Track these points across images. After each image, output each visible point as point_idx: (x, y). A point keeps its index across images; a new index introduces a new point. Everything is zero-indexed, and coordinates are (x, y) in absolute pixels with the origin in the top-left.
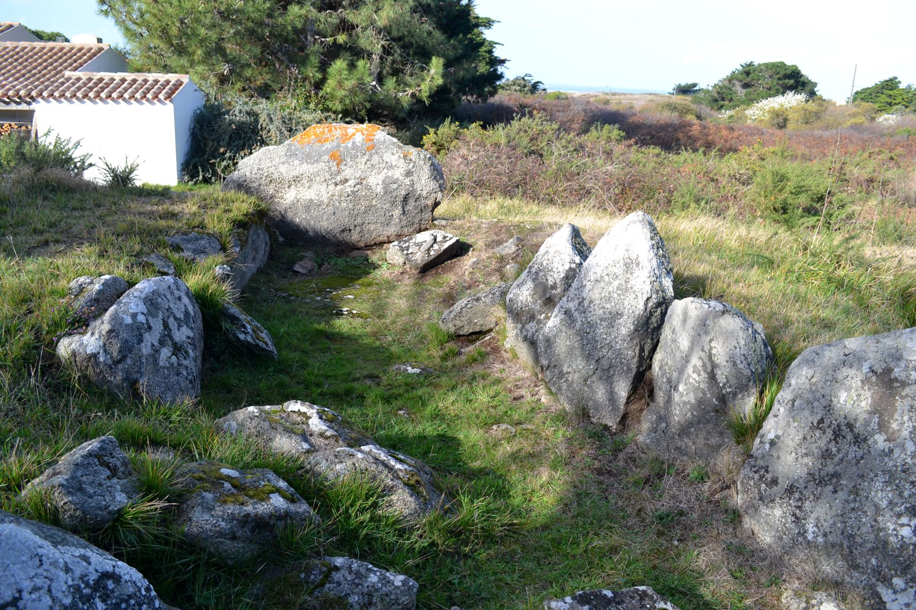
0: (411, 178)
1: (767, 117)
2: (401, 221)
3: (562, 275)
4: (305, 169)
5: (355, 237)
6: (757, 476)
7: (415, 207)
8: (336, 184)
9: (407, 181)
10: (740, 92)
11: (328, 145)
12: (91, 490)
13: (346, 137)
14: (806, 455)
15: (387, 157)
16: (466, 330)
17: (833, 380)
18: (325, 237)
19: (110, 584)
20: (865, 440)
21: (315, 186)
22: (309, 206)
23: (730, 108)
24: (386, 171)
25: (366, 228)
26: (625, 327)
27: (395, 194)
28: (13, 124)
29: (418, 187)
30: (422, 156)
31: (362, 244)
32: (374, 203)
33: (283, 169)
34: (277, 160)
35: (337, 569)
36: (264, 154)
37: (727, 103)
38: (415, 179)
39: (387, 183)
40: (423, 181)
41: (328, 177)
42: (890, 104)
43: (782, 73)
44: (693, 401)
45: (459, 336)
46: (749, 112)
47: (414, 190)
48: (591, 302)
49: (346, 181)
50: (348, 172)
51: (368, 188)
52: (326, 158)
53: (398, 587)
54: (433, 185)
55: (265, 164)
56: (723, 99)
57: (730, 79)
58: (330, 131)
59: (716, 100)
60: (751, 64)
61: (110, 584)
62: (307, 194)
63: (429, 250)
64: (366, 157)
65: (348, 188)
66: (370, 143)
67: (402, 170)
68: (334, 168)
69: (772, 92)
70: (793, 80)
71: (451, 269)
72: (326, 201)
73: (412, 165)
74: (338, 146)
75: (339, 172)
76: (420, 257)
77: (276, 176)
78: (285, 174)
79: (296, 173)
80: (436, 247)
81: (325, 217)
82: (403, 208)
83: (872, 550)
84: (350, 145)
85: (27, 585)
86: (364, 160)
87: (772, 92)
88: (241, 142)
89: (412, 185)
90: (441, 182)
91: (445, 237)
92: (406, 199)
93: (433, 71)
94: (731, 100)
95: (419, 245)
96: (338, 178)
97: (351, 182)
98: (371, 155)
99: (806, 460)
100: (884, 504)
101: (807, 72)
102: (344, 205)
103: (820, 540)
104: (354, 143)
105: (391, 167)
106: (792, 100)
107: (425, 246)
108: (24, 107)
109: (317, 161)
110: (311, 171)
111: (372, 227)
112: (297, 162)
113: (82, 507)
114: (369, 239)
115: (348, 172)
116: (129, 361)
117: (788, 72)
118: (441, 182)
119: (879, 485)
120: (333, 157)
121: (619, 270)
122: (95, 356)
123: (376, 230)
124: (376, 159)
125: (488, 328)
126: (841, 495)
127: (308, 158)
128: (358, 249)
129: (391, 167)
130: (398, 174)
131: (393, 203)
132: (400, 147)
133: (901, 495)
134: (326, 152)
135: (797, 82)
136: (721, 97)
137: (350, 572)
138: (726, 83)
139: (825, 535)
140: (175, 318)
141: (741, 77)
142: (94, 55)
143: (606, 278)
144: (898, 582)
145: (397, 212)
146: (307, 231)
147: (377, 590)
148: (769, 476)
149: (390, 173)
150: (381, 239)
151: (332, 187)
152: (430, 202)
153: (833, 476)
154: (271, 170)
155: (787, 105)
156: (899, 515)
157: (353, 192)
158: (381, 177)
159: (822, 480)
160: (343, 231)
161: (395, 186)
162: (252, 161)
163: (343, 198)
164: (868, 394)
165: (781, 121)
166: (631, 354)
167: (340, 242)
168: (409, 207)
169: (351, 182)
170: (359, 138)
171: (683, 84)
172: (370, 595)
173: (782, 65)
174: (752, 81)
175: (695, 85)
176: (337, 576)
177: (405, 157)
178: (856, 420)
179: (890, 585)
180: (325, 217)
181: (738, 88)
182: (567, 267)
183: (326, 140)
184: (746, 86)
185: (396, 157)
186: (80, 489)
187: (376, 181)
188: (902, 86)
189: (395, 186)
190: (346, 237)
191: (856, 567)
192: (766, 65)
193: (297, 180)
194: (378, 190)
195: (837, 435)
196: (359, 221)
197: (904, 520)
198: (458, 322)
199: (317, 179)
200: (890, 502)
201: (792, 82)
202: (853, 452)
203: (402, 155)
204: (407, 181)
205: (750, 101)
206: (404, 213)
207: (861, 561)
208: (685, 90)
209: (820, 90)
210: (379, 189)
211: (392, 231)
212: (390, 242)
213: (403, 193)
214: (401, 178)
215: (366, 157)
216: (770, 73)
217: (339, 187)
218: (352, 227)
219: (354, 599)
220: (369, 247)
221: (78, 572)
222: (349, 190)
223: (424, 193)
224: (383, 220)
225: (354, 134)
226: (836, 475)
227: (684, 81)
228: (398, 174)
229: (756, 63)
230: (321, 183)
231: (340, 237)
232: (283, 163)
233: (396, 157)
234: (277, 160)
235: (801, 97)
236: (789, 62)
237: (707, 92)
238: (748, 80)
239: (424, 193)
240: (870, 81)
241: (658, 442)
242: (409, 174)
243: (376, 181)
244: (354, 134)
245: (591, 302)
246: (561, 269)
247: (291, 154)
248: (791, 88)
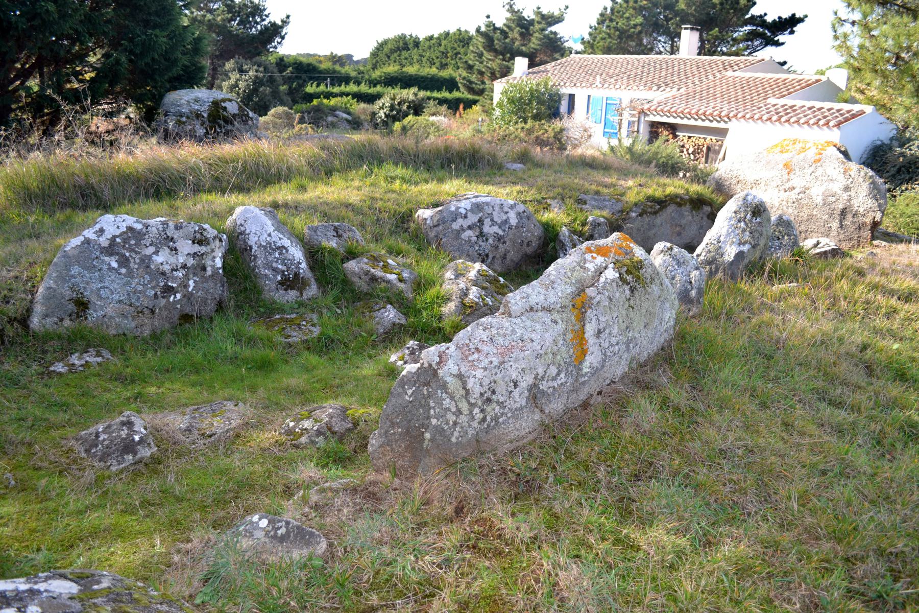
0: (849, 193)
7: (853, 223)
9: (845, 196)
12: (319, 234)
19: (284, 251)
28: (713, 138)
29: (855, 203)
30: (862, 173)
32: (815, 213)
38: (853, 193)
40: (860, 199)
47: (850, 206)
61: (284, 251)
64: (812, 169)
65: (793, 195)
68: (786, 176)
73: (851, 180)
77: (741, 178)
82: (841, 222)
85: (254, 231)
86: (810, 172)
88: (908, 177)
90: (882, 201)
92: (843, 213)
96: (787, 186)
102: (790, 211)
108: (722, 125)
113: (310, 236)
116: (441, 227)
118: (882, 201)
122: (426, 219)
124: (820, 171)
130: (837, 187)
132: (843, 163)
140: (492, 220)
142: (809, 85)
145: (835, 225)
157: (798, 200)
158: (823, 189)
161: (833, 199)
169: (797, 190)
186: (315, 231)
194: (818, 201)
203: (842, 171)
204: (845, 196)
206: (841, 227)
210: (819, 200)
213: (841, 206)
214: (839, 192)
215: (812, 169)
221: (274, 239)
224: (823, 230)
228: (837, 187)
239: (861, 210)
242: (847, 189)
243: (817, 193)
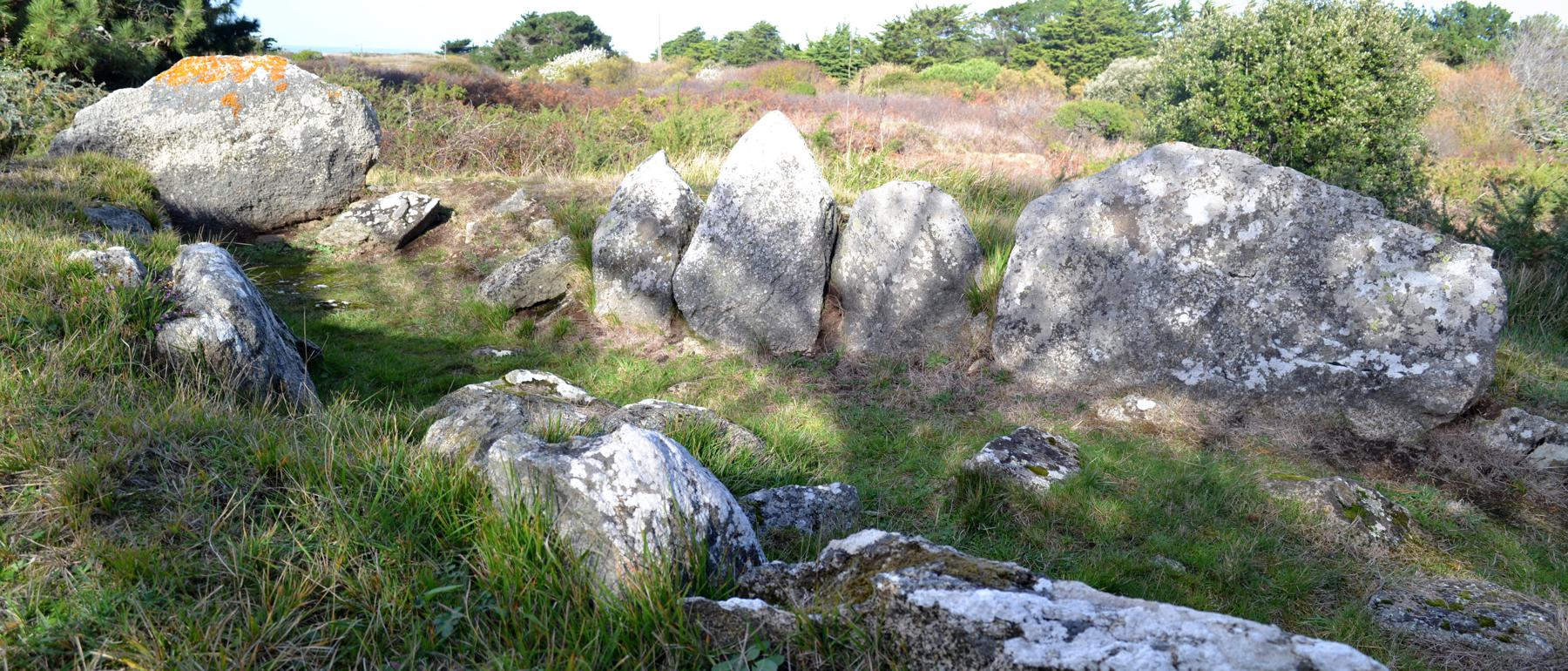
1: (566, 78)
2: (325, 187)
3: (674, 205)
4: (185, 120)
5: (258, 216)
6: (1016, 331)
7: (345, 169)
8: (233, 141)
10: (528, 49)
11: (216, 86)
13: (241, 74)
14: (1062, 294)
15: (308, 100)
16: (528, 303)
17: (1078, 219)
18: (214, 219)
20: (1121, 259)
21: (200, 146)
22: (192, 174)
23: (520, 68)
24: (305, 119)
25: (274, 202)
26: (808, 234)
27: (317, 152)
29: (349, 140)
31: (268, 226)
32: (289, 165)
33: (150, 121)
34: (139, 108)
35: (763, 503)
36: (118, 100)
37: (512, 62)
38: (346, 129)
39: (307, 137)
41: (220, 130)
42: (698, 59)
43: (574, 24)
44: (916, 287)
45: (519, 310)
46: (544, 71)
47: (345, 145)
48: (746, 219)
49: (248, 135)
50: (250, 123)
51: (281, 144)
52: (217, 103)
53: (839, 495)
54: (368, 137)
55: (121, 116)
56: (508, 58)
57: (515, 32)
58: (215, 65)
59: (499, 60)
60: (533, 16)
62: (188, 157)
63: (404, 217)
64: (277, 101)
65: (252, 145)
66: (279, 82)
67: (328, 118)
69: (564, 48)
70: (585, 34)
71: (438, 240)
72: (217, 166)
74: (233, 86)
75: (237, 124)
76: (394, 227)
77: (139, 132)
78: (153, 129)
79: (170, 127)
80: (413, 212)
81: (216, 190)
83: (1157, 347)
84: (250, 85)
86: (273, 105)
87: (565, 47)
89: (342, 138)
91: (420, 200)
92: (332, 158)
93: (188, 11)
94: (517, 58)
95: (389, 212)
96: (237, 132)
97: (256, 137)
98: (283, 98)
99: (1063, 299)
100: (1155, 305)
101: (602, 27)
102: (244, 170)
103: (1107, 357)
104: (255, 82)
105: (312, 114)
106: (589, 56)
107: (398, 213)
109: (203, 108)
110: (195, 123)
111: (284, 200)
112: (171, 112)
114: (278, 217)
115: (250, 123)
117: (581, 23)
119: (1145, 292)
120: (227, 102)
121: (777, 176)
123: (290, 203)
125: (557, 294)
126: (1113, 314)
127: (188, 104)
128: (264, 233)
129: (312, 114)
130: (322, 123)
131: (315, 165)
132: (322, 86)
133: (1167, 293)
134: (216, 95)
135: (591, 36)
136: (505, 55)
137: (780, 500)
138: (509, 38)
139: (1109, 352)
141: (527, 30)
143: (761, 189)
144: (1187, 362)
145: (320, 177)
146: (188, 213)
147: (819, 506)
148: (1029, 327)
149: (312, 122)
150: (296, 216)
151: (226, 146)
152: (364, 161)
153: (1096, 302)
154: (130, 124)
155: (587, 63)
156: (1173, 309)
158: (299, 128)
159: (1095, 308)
160: (242, 209)
161: (319, 140)
162: (98, 113)
163: (243, 161)
164: (1109, 223)
165: (582, 77)
166: (818, 262)
167: (237, 225)
168: (336, 170)
169: (256, 137)
170: (262, 75)
171: (453, 41)
172: (814, 514)
173: (570, 16)
174: (539, 35)
175: (467, 42)
176: (769, 509)
177: (332, 99)
178: (1106, 246)
179: (1182, 367)
180: (216, 190)
181: (524, 43)
182: (677, 195)
183: (213, 78)
184: (533, 41)
185: (319, 99)
187: (291, 134)
188: (707, 37)
189: (319, 140)
190: (245, 216)
191: (1145, 367)
192: (555, 15)
193: (172, 137)
195: (1090, 264)
196: (266, 192)
197: (1178, 311)
198: (516, 292)
199: (204, 134)
200: (1161, 302)
201: (586, 35)
202: (1112, 274)
204: (335, 133)
205: (541, 60)
207: (1148, 361)
208: (456, 48)
209: (616, 45)
210: (297, 145)
211: (312, 204)
212: (307, 220)
213: (330, 149)
214: (327, 128)
216: (560, 24)
217: (237, 146)
218: (255, 203)
219: (802, 524)
220: (277, 229)
222: (253, 148)
223: (357, 148)
225: (253, 70)
226: (1102, 299)
227: (455, 37)
228: (322, 123)
229: (540, 14)
230: (210, 140)
231: (238, 218)
232: (149, 113)
233: (319, 99)
234: (139, 108)
235: (601, 52)
236: (580, 13)
237: (486, 49)
238: (535, 34)
239: (357, 148)
240: (674, 33)
241: (878, 345)
242: (337, 122)
243: (291, 134)
244: (253, 70)
245: (746, 219)
246: (669, 199)
247: (159, 101)
248: (588, 42)
